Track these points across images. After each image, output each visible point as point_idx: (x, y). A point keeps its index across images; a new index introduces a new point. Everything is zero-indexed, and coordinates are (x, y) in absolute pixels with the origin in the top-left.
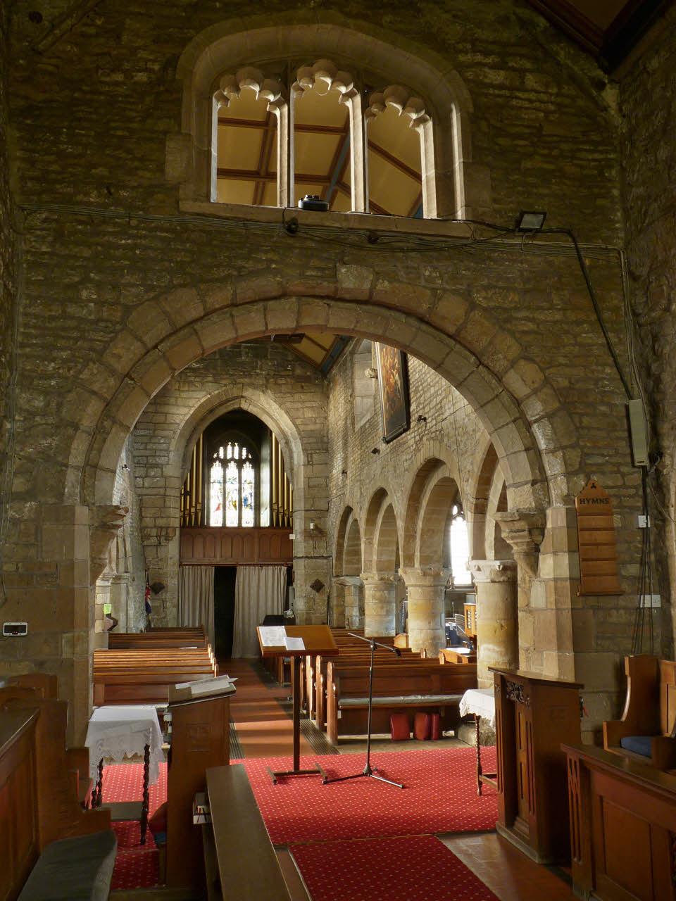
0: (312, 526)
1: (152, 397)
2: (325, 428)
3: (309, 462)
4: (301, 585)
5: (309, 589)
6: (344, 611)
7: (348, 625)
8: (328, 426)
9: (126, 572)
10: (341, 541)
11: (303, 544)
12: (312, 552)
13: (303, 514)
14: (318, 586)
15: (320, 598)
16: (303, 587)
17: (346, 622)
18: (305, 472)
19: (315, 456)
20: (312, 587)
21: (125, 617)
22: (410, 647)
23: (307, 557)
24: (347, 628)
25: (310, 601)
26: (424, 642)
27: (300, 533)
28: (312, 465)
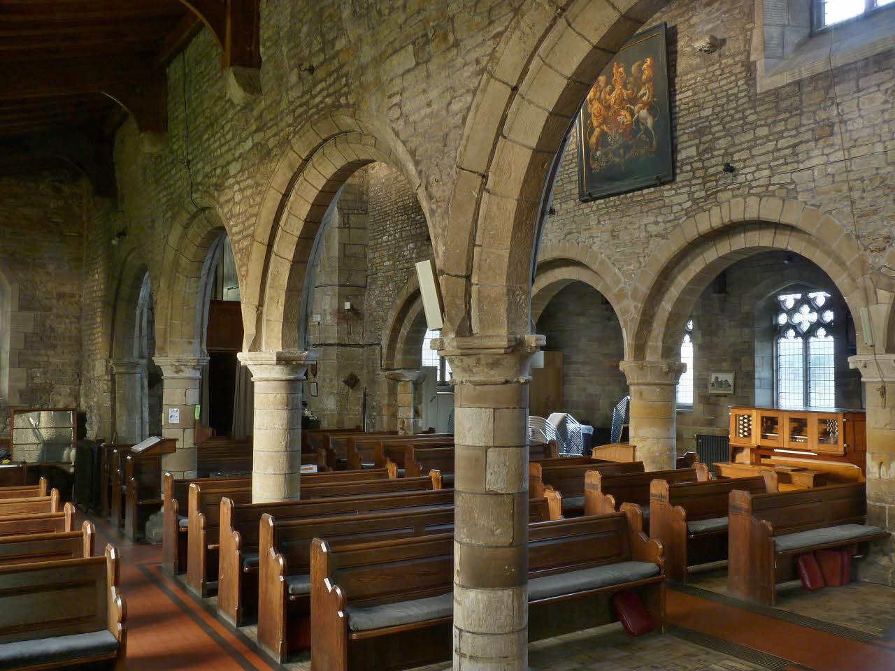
0: (347, 305)
1: (128, 111)
2: (365, 181)
3: (345, 224)
4: (331, 380)
5: (342, 383)
6: (397, 411)
7: (402, 429)
8: (368, 182)
9: (142, 357)
10: (398, 326)
11: (336, 328)
12: (346, 339)
13: (337, 290)
14: (352, 382)
15: (356, 396)
16: (335, 382)
17: (399, 426)
18: (340, 237)
19: (352, 218)
20: (346, 382)
21: (140, 421)
22: (638, 460)
23: (340, 345)
24: (401, 433)
25: (342, 400)
26: (661, 454)
27: (331, 314)
28: (349, 228)
